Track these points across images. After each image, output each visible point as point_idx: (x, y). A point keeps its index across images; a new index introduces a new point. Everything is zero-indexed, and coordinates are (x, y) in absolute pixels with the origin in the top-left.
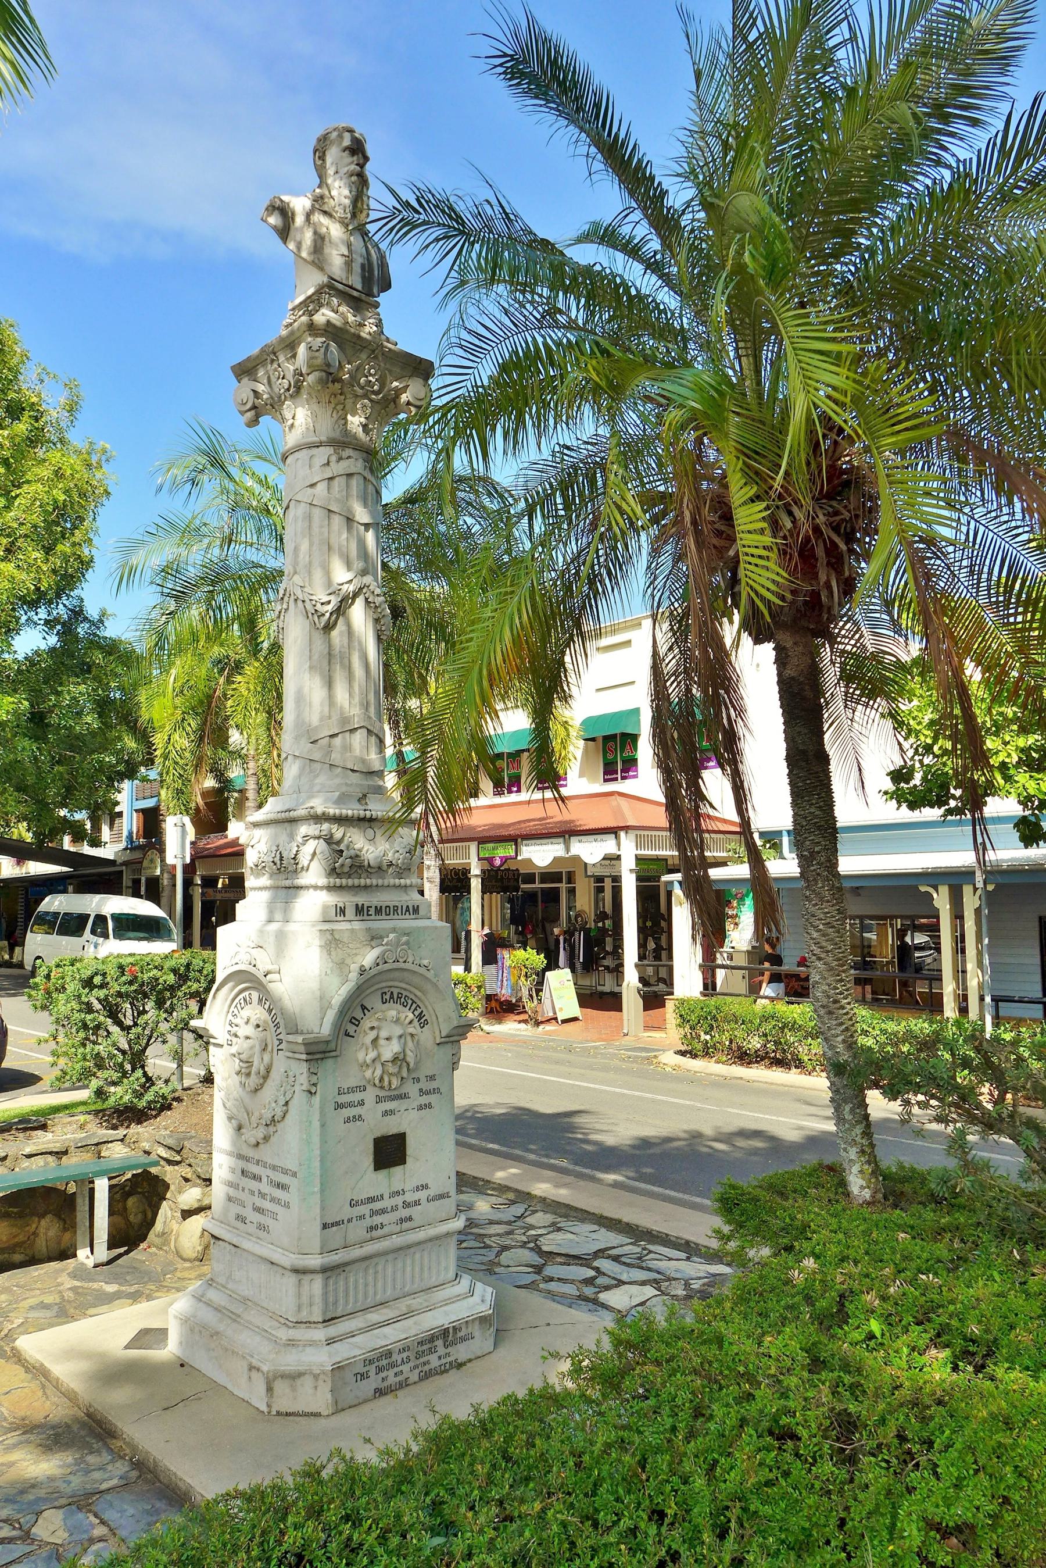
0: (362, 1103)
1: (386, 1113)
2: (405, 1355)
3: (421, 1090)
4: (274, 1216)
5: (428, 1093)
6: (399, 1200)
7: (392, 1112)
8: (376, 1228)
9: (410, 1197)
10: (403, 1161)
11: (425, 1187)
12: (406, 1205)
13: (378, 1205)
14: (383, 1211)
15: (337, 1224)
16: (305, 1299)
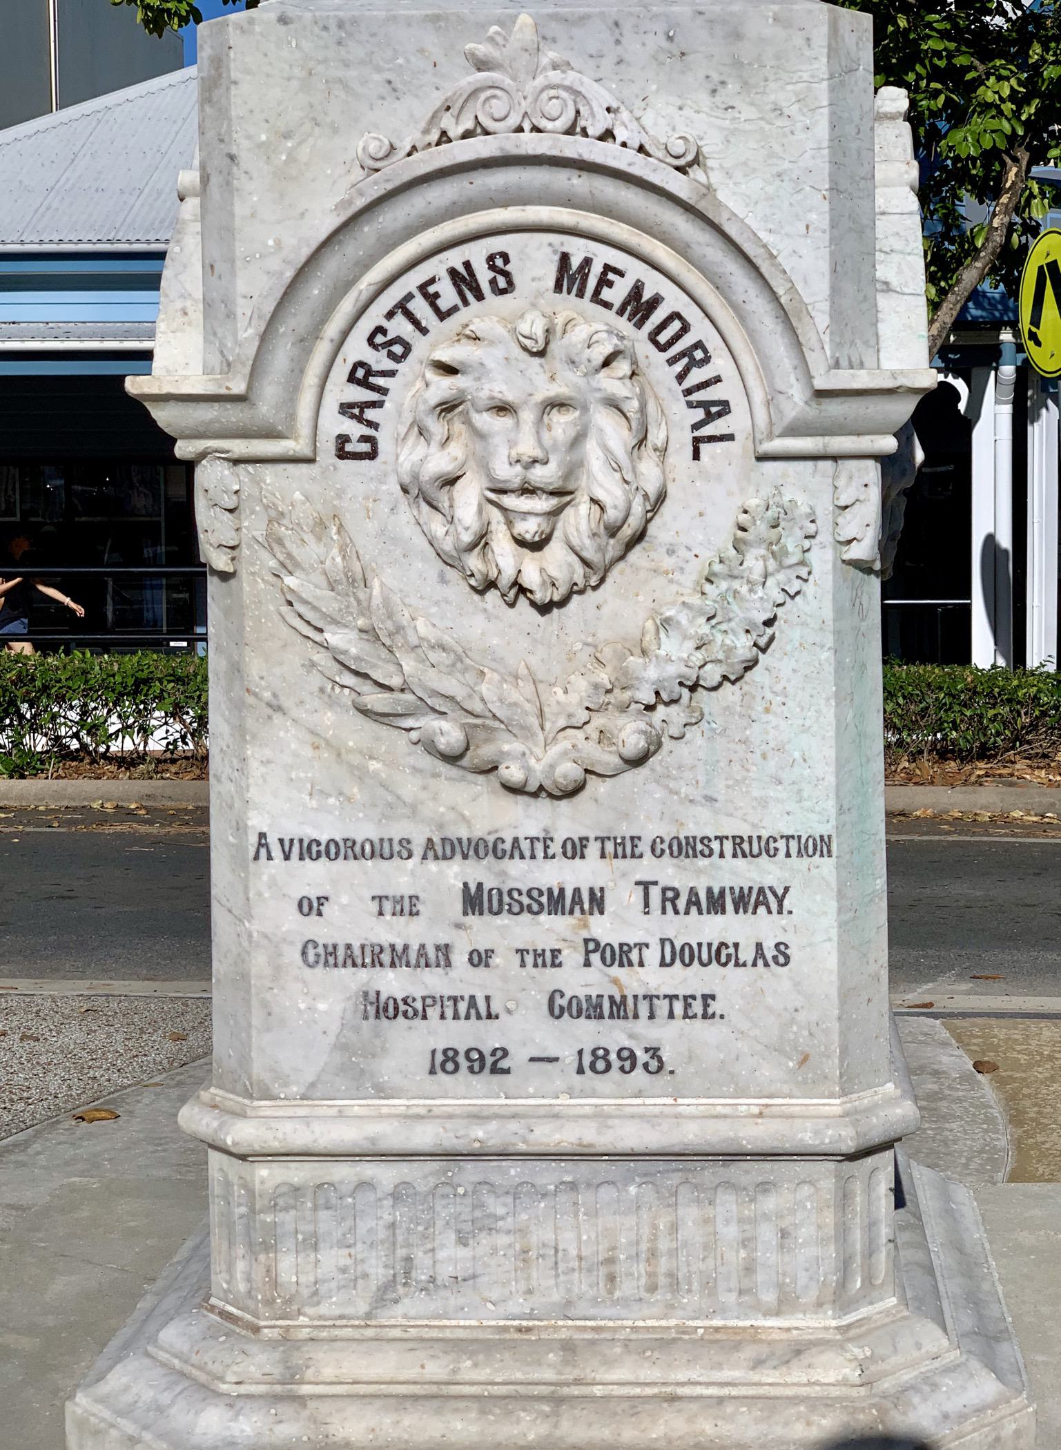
4: (701, 1007)
16: (857, 1237)
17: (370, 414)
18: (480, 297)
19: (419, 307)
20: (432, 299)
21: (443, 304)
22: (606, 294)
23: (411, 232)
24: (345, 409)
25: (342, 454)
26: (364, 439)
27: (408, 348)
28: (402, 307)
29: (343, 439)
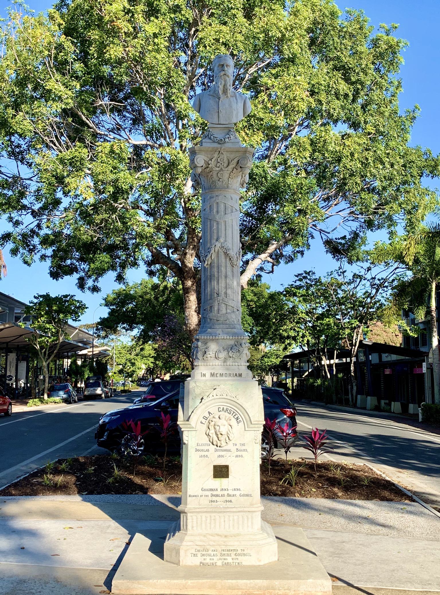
0: (208, 450)
2: (215, 553)
3: (237, 449)
6: (226, 493)
7: (222, 456)
8: (214, 501)
9: (231, 492)
11: (239, 490)
12: (229, 495)
13: (215, 493)
14: (217, 496)
15: (195, 496)
23: (245, 417)
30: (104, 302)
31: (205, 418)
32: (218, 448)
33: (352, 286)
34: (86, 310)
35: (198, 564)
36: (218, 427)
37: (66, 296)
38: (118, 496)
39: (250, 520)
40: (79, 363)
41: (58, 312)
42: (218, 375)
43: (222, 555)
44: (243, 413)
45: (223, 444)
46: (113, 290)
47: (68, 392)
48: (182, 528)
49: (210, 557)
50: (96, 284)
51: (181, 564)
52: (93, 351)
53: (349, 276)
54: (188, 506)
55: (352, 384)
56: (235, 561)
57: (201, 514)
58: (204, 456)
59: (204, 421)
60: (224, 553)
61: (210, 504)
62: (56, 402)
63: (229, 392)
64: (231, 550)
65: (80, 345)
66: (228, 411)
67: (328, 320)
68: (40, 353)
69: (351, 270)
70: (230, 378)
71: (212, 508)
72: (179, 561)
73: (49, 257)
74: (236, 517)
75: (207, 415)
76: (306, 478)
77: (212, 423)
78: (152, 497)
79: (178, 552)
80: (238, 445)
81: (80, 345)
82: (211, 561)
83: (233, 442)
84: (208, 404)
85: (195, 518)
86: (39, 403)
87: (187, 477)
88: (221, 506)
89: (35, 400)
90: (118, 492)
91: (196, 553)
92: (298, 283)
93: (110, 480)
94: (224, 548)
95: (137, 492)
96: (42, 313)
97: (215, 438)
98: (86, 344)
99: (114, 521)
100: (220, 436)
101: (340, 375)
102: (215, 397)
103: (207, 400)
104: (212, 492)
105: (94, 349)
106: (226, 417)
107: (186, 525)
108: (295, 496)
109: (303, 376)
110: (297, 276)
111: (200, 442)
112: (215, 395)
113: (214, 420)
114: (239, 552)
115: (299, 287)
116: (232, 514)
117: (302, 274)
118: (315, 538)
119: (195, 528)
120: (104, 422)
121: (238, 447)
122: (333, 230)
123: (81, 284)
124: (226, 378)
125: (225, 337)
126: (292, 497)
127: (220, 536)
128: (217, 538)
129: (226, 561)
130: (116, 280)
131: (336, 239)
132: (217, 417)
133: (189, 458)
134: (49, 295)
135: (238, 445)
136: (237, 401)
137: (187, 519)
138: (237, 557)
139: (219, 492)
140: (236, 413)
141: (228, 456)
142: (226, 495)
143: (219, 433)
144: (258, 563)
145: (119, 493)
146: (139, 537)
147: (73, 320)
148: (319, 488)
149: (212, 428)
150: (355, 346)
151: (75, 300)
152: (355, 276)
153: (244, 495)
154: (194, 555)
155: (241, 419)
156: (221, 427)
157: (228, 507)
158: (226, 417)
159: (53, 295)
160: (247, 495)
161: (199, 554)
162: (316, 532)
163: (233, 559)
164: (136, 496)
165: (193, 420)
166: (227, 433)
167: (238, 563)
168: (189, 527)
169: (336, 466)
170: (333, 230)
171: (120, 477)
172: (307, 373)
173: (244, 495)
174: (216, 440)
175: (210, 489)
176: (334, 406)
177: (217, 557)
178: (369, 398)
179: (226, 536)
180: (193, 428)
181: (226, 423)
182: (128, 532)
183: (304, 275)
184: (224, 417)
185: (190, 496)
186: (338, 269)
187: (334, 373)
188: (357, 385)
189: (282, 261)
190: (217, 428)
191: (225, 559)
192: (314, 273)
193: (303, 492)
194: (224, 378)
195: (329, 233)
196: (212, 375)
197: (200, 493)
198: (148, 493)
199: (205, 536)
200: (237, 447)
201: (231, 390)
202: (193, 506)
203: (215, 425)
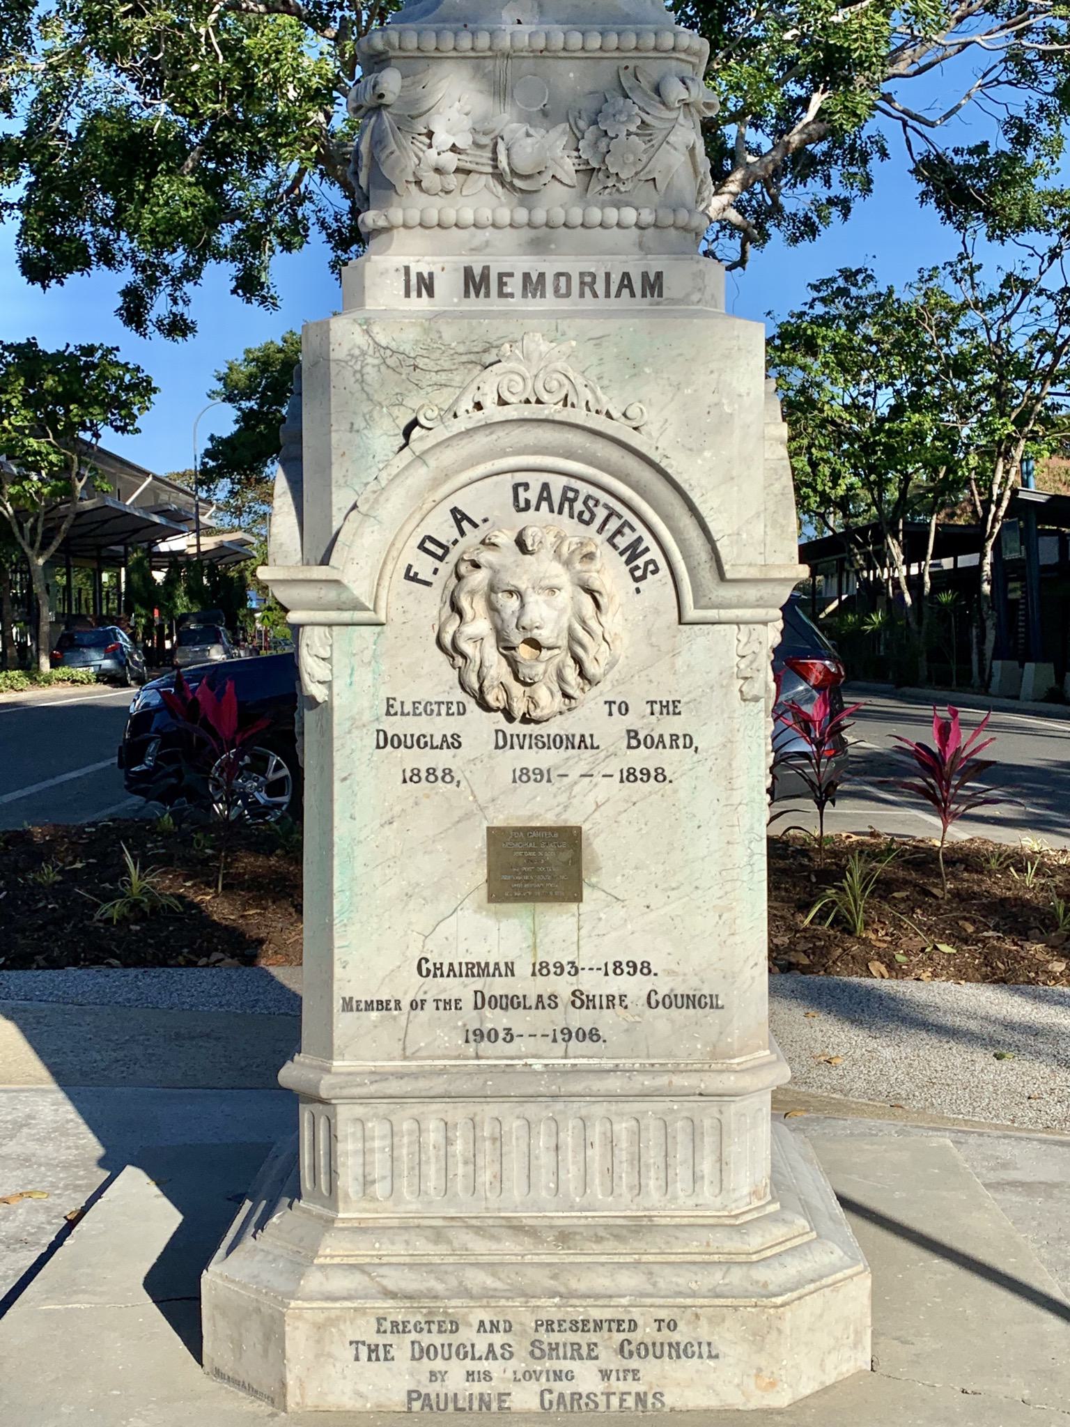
0: (453, 742)
1: (523, 776)
2: (498, 1339)
3: (632, 734)
5: (656, 743)
6: (563, 986)
7: (542, 775)
8: (492, 1036)
9: (591, 983)
10: (574, 895)
11: (646, 968)
12: (581, 1000)
13: (498, 986)
14: (512, 1002)
15: (382, 1005)
17: (544, 505)
18: (628, 562)
19: (613, 525)
20: (619, 532)
21: (618, 540)
22: (507, 290)
23: (681, 542)
24: (545, 487)
25: (516, 487)
26: (527, 502)
27: (587, 523)
28: (612, 513)
29: (526, 486)
30: (219, 386)
31: (432, 547)
32: (517, 728)
33: (999, 311)
34: (153, 397)
35: (397, 1399)
36: (514, 603)
37: (89, 350)
38: (132, 972)
39: (709, 1142)
40: (159, 576)
41: (64, 399)
42: (514, 286)
43: (538, 1350)
44: (666, 519)
45: (547, 700)
46: (248, 351)
47: (116, 654)
48: (307, 1184)
49: (470, 1365)
50: (180, 308)
51: (291, 1403)
52: (198, 545)
53: (990, 282)
54: (337, 1064)
55: (983, 621)
56: (618, 1386)
57: (416, 1110)
58: (431, 771)
59: (424, 565)
60: (555, 1337)
61: (471, 1049)
62: (74, 682)
63: (579, 382)
64: (598, 1325)
65: (156, 519)
66: (579, 506)
67: (916, 417)
68: (16, 530)
69: (999, 258)
70: (589, 302)
71: (480, 1070)
72: (283, 1385)
73: (12, 207)
74: (622, 1128)
75: (445, 531)
76: (903, 900)
77: (478, 579)
78: (273, 978)
79: (274, 1335)
80: (639, 707)
81: (156, 519)
82: (477, 1388)
83: (605, 690)
84: (448, 457)
85: (377, 1128)
86: (26, 681)
87: (329, 895)
88: (538, 1064)
89: (10, 673)
90: (134, 958)
91: (381, 1340)
92: (820, 309)
93: (114, 910)
94: (550, 1309)
95: (215, 956)
96: (14, 402)
97: (497, 669)
98: (178, 521)
99: (61, 1096)
100: (524, 652)
101: (945, 598)
102: (492, 412)
103: (441, 433)
104: (478, 983)
105: (203, 540)
106: (561, 538)
107: (332, 1173)
108: (870, 975)
109: (822, 616)
110: (816, 288)
111: (407, 694)
112: (489, 401)
113: (485, 556)
114: (647, 1332)
115: (826, 321)
116: (599, 1110)
117: (834, 280)
118: (1013, 1184)
119: (380, 1189)
120: (146, 705)
121: (637, 719)
122: (947, 116)
123: (133, 310)
124: (564, 305)
125: (558, 41)
126: (855, 979)
127: (532, 1232)
128: (510, 1247)
129: (564, 1387)
130: (237, 288)
131: (956, 151)
132: (505, 539)
133: (337, 786)
134: (35, 345)
135: (639, 707)
136: (635, 440)
137: (332, 1137)
138: (634, 1363)
139: (524, 984)
140: (629, 505)
141: (574, 775)
142: (565, 995)
143: (516, 638)
144: (760, 1400)
145: (140, 963)
146: (135, 1183)
147: (117, 429)
148: (966, 942)
149: (474, 607)
150: (998, 505)
151: (117, 364)
152: (1009, 281)
153: (670, 1001)
154: (373, 1349)
155: (655, 553)
156: (531, 598)
157: (575, 1071)
158: (561, 538)
159: (49, 345)
160: (693, 1001)
161: (402, 1347)
162: (1005, 1150)
163: (605, 1375)
164: (205, 972)
165: (357, 565)
166: (573, 638)
167: (641, 1399)
168: (348, 1181)
169: (1009, 857)
170: (947, 116)
171: (153, 899)
172: (836, 603)
173: (670, 1001)
174: (506, 678)
175: (470, 966)
176: (927, 692)
177: (513, 1364)
178: (1030, 667)
179: (564, 1237)
180: (360, 607)
181: (562, 577)
182: (99, 1151)
183: (841, 283)
184: (550, 539)
185: (348, 1005)
186: (954, 259)
187: (927, 590)
188: (997, 626)
189: (777, 235)
190: (510, 605)
191: (558, 1376)
192: (871, 277)
193: (900, 958)
194: (549, 302)
195: (932, 125)
196: (475, 283)
197: (410, 986)
198: (262, 963)
199: (438, 1235)
200: (631, 721)
201: (593, 373)
202: (370, 1065)
203: (492, 588)
